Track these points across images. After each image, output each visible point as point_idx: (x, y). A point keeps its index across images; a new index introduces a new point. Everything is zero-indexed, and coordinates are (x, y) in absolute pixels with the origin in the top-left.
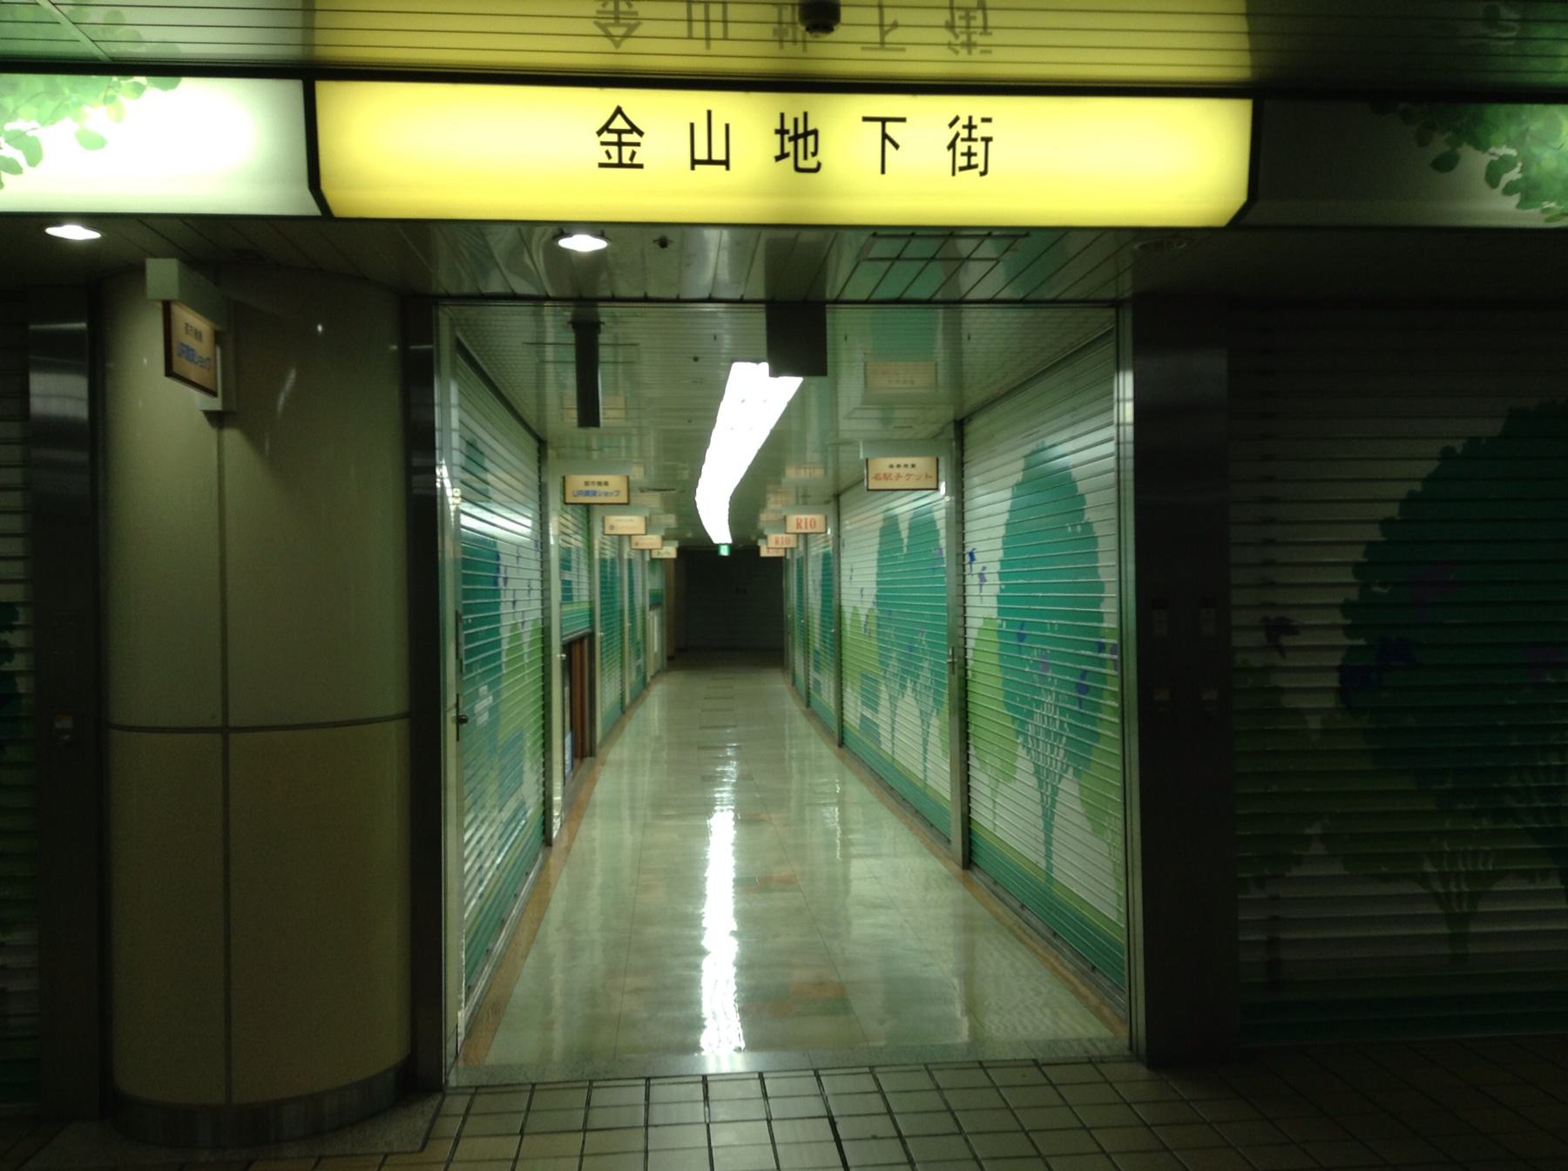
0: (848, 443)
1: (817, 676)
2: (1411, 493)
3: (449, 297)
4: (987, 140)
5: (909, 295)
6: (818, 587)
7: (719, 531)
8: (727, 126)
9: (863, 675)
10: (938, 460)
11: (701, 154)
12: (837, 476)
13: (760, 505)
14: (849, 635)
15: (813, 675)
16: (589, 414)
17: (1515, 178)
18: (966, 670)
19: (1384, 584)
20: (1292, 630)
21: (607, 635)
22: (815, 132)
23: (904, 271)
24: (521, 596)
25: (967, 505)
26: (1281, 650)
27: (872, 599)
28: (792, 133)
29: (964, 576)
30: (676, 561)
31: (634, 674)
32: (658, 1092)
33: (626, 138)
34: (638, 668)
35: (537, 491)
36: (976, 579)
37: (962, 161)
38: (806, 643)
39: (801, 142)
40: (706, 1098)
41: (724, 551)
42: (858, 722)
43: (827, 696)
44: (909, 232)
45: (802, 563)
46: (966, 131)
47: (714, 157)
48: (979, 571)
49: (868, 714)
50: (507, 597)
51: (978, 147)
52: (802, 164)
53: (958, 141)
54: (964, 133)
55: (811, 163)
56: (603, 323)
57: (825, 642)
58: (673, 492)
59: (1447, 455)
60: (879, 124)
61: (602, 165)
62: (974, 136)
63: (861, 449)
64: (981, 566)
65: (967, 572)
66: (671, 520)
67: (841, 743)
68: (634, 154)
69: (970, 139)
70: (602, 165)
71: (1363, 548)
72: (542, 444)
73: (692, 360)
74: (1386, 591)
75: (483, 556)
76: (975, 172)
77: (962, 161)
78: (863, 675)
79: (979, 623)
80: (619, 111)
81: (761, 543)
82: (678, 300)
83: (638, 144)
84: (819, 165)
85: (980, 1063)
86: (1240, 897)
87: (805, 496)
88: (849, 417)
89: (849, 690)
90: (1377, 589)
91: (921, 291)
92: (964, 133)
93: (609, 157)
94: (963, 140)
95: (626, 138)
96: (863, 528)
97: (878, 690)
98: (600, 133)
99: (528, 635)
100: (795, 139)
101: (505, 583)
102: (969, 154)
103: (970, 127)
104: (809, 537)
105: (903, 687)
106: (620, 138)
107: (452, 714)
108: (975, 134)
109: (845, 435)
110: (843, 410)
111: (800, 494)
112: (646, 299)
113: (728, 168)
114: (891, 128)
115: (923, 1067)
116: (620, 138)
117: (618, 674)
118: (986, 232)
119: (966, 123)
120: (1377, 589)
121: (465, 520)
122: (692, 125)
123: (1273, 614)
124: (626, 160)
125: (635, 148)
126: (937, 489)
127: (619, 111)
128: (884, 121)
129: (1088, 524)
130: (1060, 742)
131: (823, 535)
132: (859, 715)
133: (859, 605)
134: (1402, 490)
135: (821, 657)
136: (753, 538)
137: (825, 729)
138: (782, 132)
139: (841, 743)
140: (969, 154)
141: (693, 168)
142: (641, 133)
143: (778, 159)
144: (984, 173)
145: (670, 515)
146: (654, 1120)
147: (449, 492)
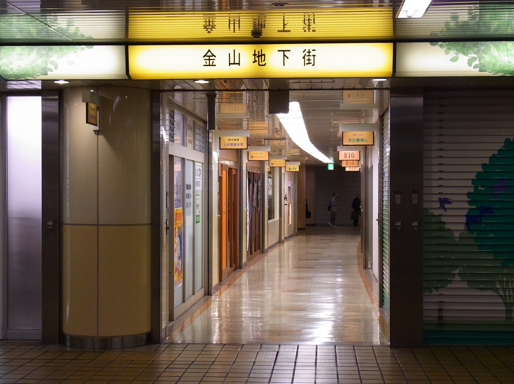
4: (314, 56)
11: (232, 62)
17: (477, 64)
22: (264, 55)
26: (445, 209)
28: (258, 55)
33: (211, 58)
37: (307, 62)
39: (260, 58)
51: (312, 58)
52: (260, 63)
53: (306, 56)
54: (307, 54)
55: (263, 63)
60: (283, 52)
61: (204, 65)
62: (310, 55)
68: (213, 62)
69: (309, 56)
70: (204, 65)
71: (476, 174)
76: (311, 65)
77: (307, 62)
80: (209, 51)
83: (214, 59)
84: (265, 64)
92: (307, 54)
93: (206, 63)
94: (307, 56)
95: (211, 58)
98: (204, 57)
100: (258, 57)
102: (309, 60)
103: (309, 52)
106: (209, 58)
108: (311, 54)
113: (239, 65)
114: (286, 53)
116: (209, 58)
119: (308, 51)
123: (442, 197)
124: (211, 64)
125: (214, 61)
127: (209, 51)
128: (284, 51)
134: (490, 154)
138: (255, 55)
140: (309, 60)
141: (230, 65)
142: (215, 57)
143: (254, 62)
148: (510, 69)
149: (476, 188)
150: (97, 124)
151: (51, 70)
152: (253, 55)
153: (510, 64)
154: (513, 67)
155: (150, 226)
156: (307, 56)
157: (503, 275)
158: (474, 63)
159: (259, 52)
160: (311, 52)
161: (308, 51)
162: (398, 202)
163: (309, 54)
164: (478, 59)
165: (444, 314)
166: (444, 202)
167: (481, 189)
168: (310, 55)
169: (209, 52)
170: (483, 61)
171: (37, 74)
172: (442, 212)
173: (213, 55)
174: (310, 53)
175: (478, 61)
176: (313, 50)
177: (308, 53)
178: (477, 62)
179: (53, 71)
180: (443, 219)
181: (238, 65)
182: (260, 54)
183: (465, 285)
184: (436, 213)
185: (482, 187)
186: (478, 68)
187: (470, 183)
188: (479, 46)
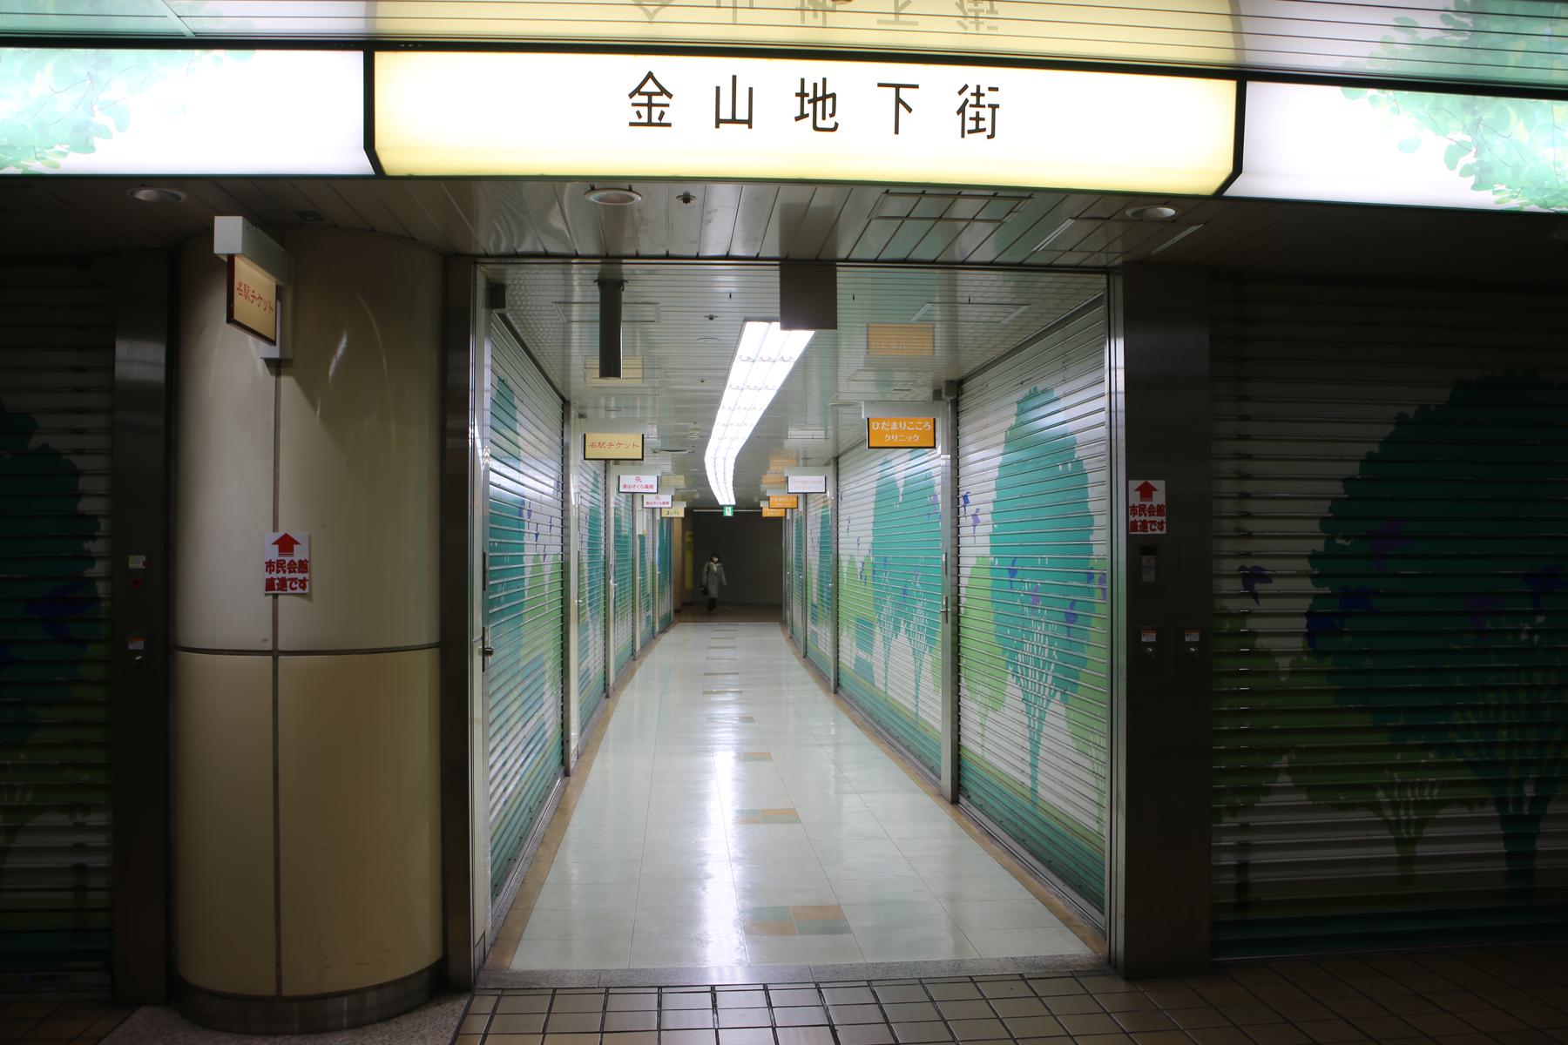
0: (848, 404)
1: (814, 628)
2: (1370, 453)
3: (487, 256)
4: (994, 107)
5: (915, 255)
6: (816, 544)
7: (725, 495)
8: (751, 90)
9: (858, 620)
10: (934, 420)
11: (726, 113)
12: (837, 440)
13: (764, 468)
14: (845, 587)
15: (811, 627)
16: (610, 366)
17: (1470, 163)
18: (959, 607)
19: (1346, 538)
20: (1266, 579)
21: (620, 586)
22: (833, 96)
23: (912, 229)
24: (543, 529)
25: (962, 462)
26: (1255, 596)
27: (868, 546)
28: (811, 97)
29: (959, 519)
30: (683, 519)
31: (644, 623)
32: (670, 1000)
33: (655, 100)
34: (648, 617)
35: (560, 418)
36: (970, 520)
37: (970, 125)
38: (804, 600)
39: (820, 104)
40: (714, 1006)
41: (728, 513)
42: (854, 662)
43: (824, 645)
44: (920, 190)
45: (802, 523)
46: (975, 98)
47: (738, 117)
48: (973, 513)
49: (863, 655)
50: (530, 529)
51: (986, 113)
52: (820, 124)
53: (967, 107)
54: (973, 100)
55: (829, 123)
56: (626, 281)
57: (822, 596)
58: (684, 452)
59: (1401, 420)
60: (894, 89)
61: (632, 124)
62: (981, 103)
63: (863, 410)
64: (974, 508)
65: (962, 514)
66: (680, 481)
67: (837, 687)
68: (662, 114)
69: (978, 105)
70: (632, 124)
71: (1329, 503)
72: (566, 404)
73: (707, 319)
74: (1349, 543)
75: (510, 517)
76: (984, 135)
77: (970, 125)
78: (858, 620)
79: (973, 561)
80: (650, 75)
81: (763, 504)
82: (698, 257)
83: (667, 105)
84: (836, 125)
85: (970, 977)
86: (1214, 825)
87: (805, 459)
88: (851, 379)
89: (845, 633)
90: (1340, 542)
91: (925, 252)
92: (973, 100)
93: (640, 116)
94: (971, 106)
95: (655, 100)
96: (861, 485)
97: (872, 633)
98: (631, 95)
99: (550, 569)
100: (814, 101)
101: (529, 517)
102: (977, 119)
103: (978, 94)
104: (809, 497)
105: (897, 628)
106: (650, 100)
107: (478, 647)
108: (983, 101)
109: (843, 398)
110: (844, 372)
111: (801, 457)
112: (668, 257)
113: (750, 127)
114: (904, 93)
115: (917, 981)
116: (650, 100)
117: (630, 619)
118: (992, 193)
119: (975, 91)
120: (1340, 542)
121: (493, 477)
122: (718, 89)
123: (1250, 563)
124: (655, 119)
125: (664, 109)
126: (934, 447)
127: (650, 75)
128: (898, 87)
129: (1079, 461)
130: (1049, 669)
131: (823, 495)
132: (854, 656)
133: (855, 553)
134: (1363, 450)
135: (819, 611)
136: (756, 500)
137: (820, 676)
138: (802, 95)
139: (837, 687)
140: (977, 119)
141: (717, 126)
142: (670, 96)
143: (797, 119)
144: (991, 136)
145: (680, 476)
146: (667, 1024)
147: (480, 452)
148: (1558, 182)
149: (1329, 540)
150: (273, 338)
151: (105, 134)
152: (797, 95)
153: (1558, 170)
154: (1567, 179)
155: (436, 651)
156: (971, 106)
157: (1393, 767)
158: (1461, 159)
159: (815, 85)
160: (983, 95)
161: (975, 91)
162: (1149, 577)
163: (978, 100)
164: (1474, 150)
165: (1253, 877)
166: (1253, 577)
167: (1343, 542)
168: (981, 103)
169: (650, 80)
170: (1486, 157)
171: (58, 148)
172: (1248, 605)
173: (663, 92)
174: (981, 98)
175: (1473, 154)
176: (991, 89)
177: (975, 98)
178: (1469, 159)
179: (111, 137)
180: (1253, 624)
181: (747, 125)
182: (820, 94)
183: (1301, 798)
184: (1232, 605)
185: (1344, 537)
186: (1473, 177)
187: (1314, 526)
188: (1477, 108)
